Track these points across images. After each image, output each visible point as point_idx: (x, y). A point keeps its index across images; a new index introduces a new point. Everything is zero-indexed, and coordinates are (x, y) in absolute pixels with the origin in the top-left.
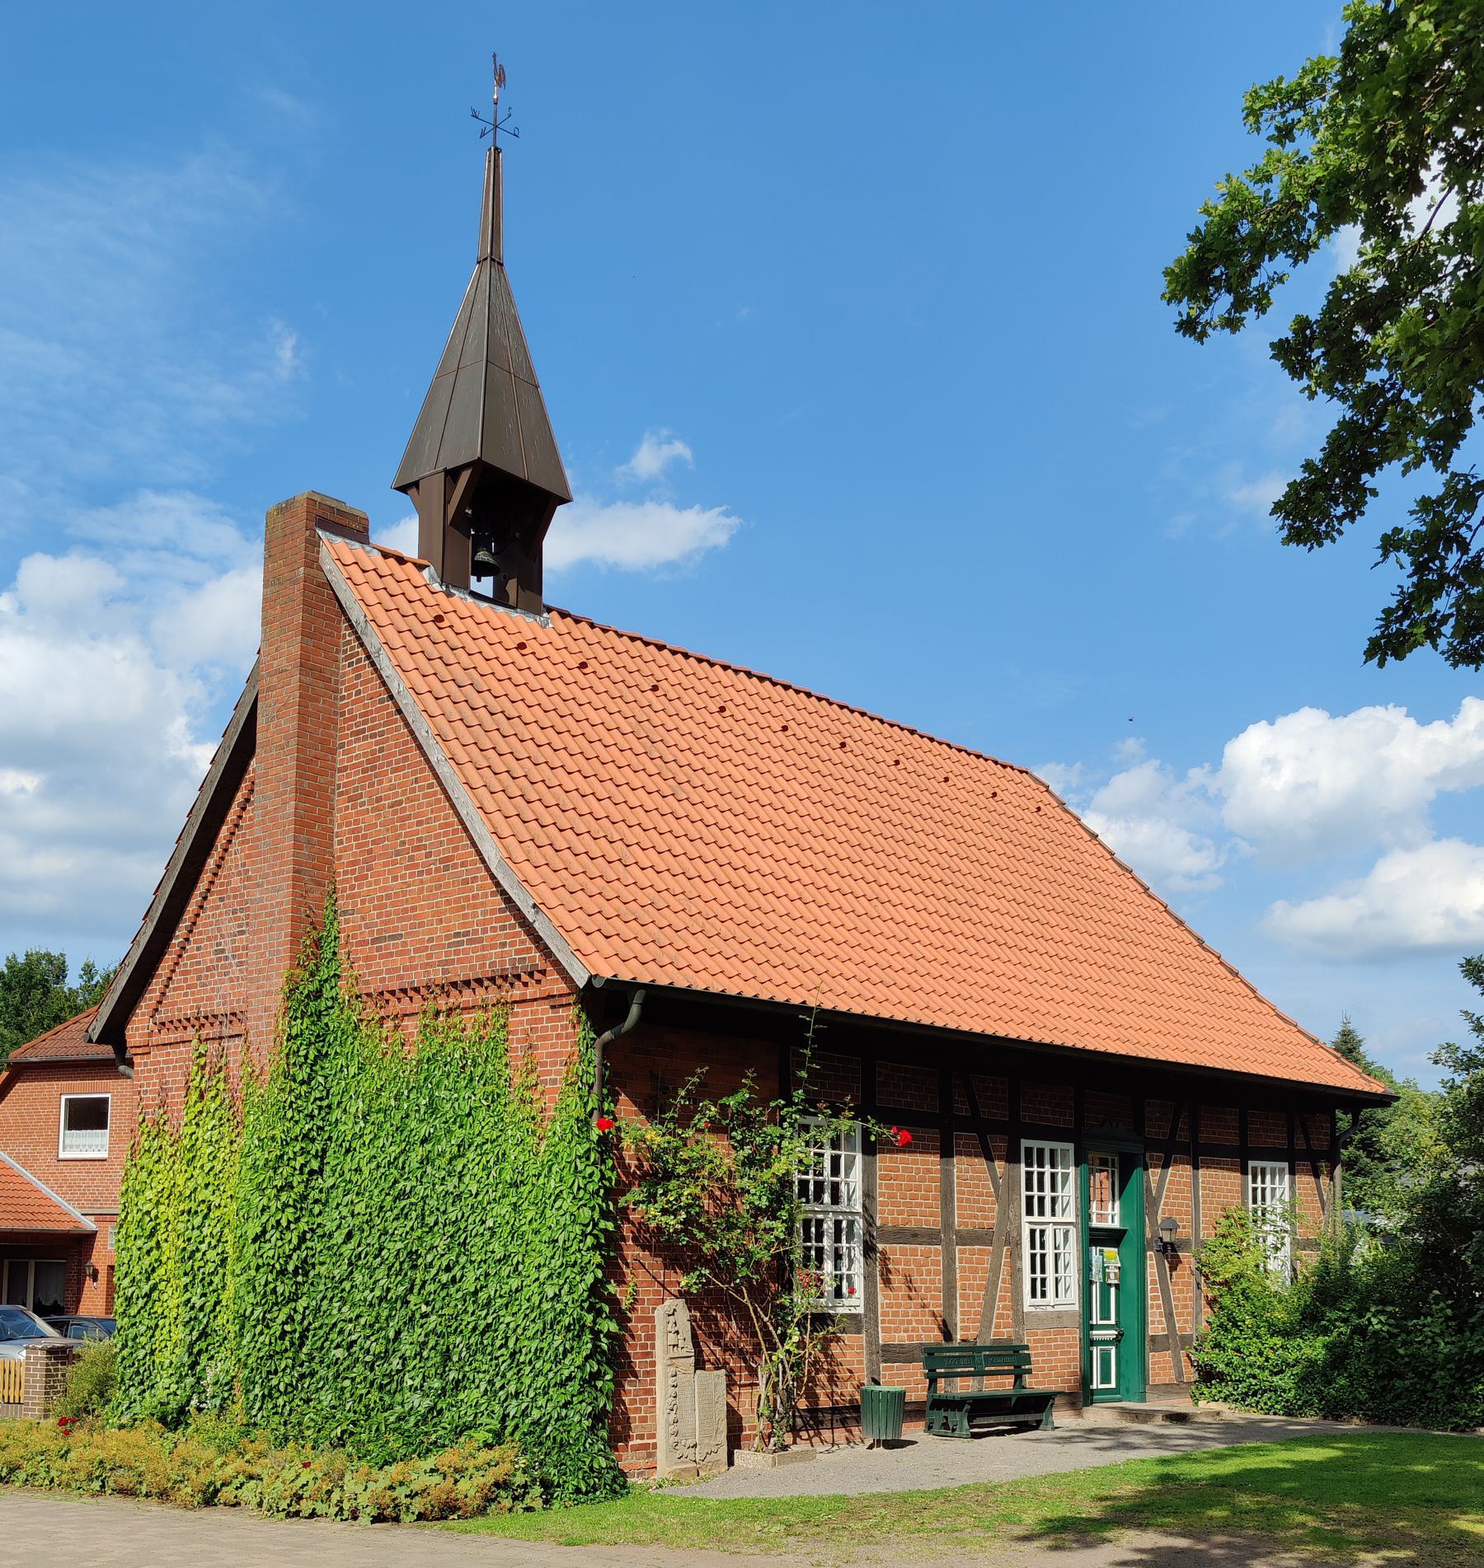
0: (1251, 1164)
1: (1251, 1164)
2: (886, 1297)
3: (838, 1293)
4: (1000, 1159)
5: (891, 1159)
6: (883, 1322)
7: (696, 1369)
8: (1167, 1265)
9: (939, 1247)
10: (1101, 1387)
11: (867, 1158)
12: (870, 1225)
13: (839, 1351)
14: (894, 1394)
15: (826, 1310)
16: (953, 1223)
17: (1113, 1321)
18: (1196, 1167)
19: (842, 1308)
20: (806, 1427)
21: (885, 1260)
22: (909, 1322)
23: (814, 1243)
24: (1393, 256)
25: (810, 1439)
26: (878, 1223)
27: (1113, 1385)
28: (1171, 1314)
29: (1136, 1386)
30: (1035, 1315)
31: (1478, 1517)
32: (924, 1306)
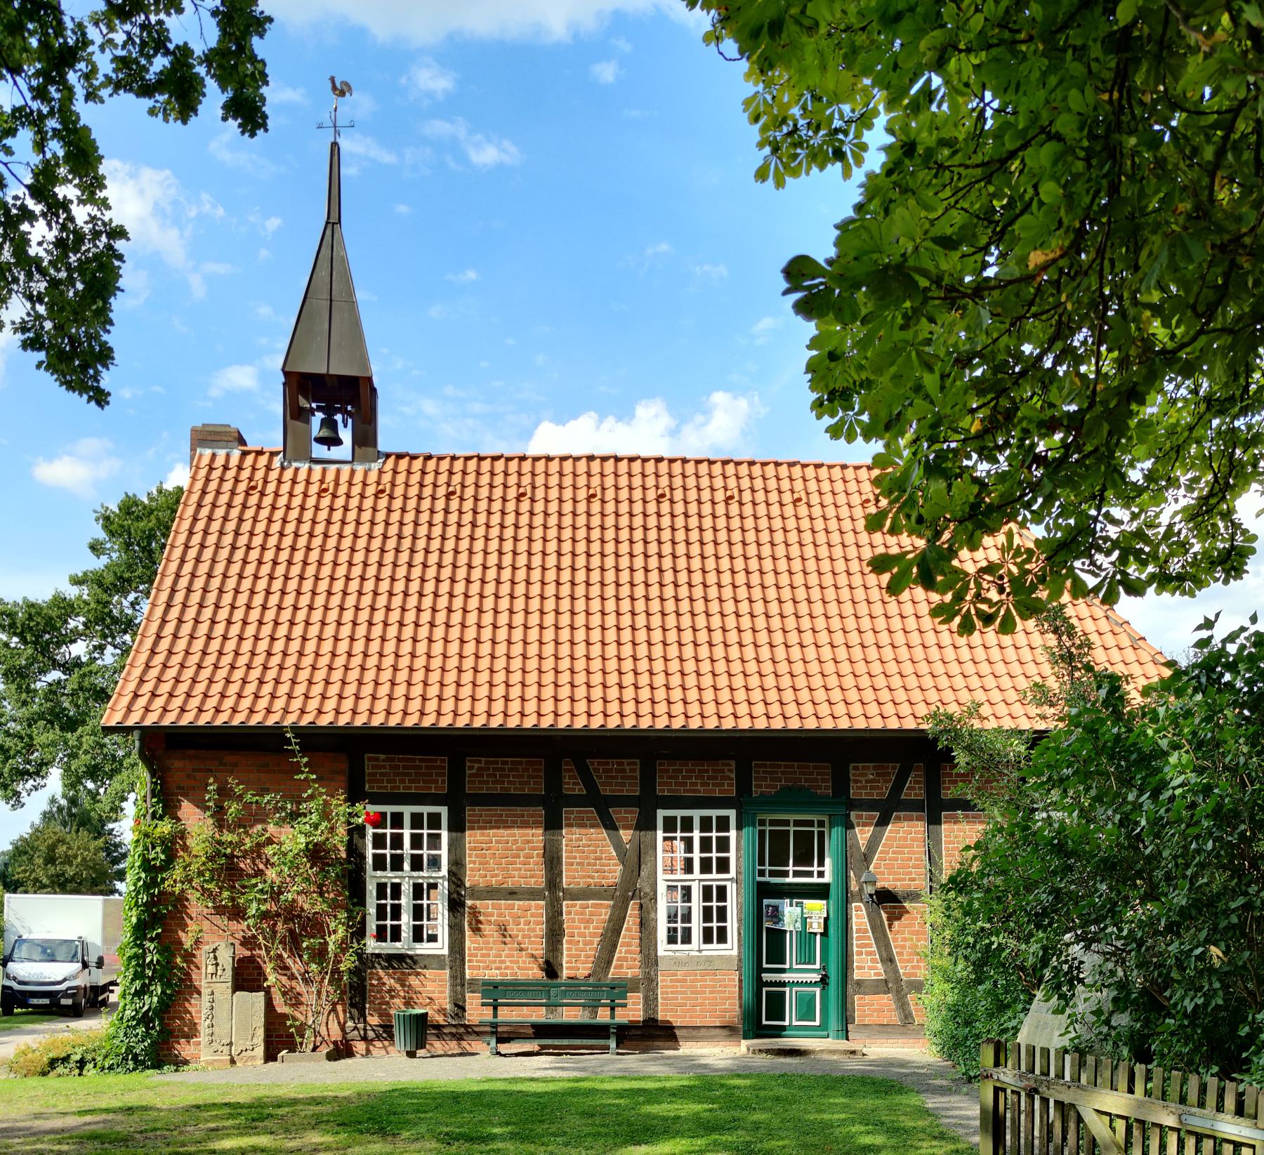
0: (661, 814)
1: (661, 814)
2: (472, 942)
3: (418, 935)
4: (626, 828)
5: (483, 835)
6: (470, 961)
7: (234, 992)
8: (884, 916)
9: (543, 903)
10: (795, 1023)
11: (454, 834)
12: (458, 886)
13: (417, 982)
14: (417, 1016)
15: (403, 951)
16: (561, 881)
17: (817, 966)
18: (553, 824)
19: (424, 949)
20: (378, 1037)
21: (475, 913)
22: (502, 962)
23: (389, 901)
24: (70, 177)
25: (385, 1047)
26: (467, 885)
27: (765, 1022)
28: (891, 960)
29: (834, 1024)
30: (671, 958)
31: (654, 1109)
32: (521, 950)
